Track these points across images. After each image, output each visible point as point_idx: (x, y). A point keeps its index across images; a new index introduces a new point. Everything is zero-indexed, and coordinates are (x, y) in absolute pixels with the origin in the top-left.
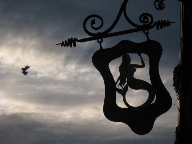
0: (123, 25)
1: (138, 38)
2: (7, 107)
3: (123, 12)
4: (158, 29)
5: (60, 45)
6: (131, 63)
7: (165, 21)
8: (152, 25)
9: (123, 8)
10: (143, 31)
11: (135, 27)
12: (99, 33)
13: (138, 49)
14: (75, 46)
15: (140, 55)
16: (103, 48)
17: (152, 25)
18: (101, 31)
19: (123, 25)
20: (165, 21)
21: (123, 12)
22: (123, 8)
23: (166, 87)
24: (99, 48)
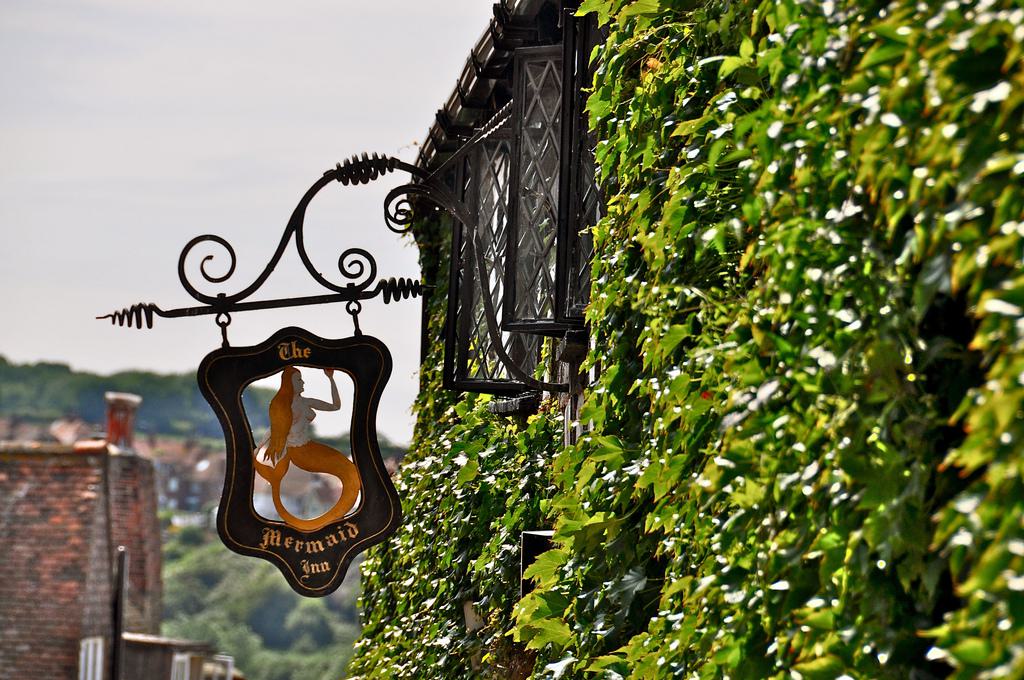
0: (292, 278)
1: (331, 323)
2: (142, 590)
3: (294, 233)
4: (387, 301)
5: (110, 318)
6: (302, 394)
7: (409, 280)
8: (372, 288)
9: (296, 223)
10: (215, 315)
11: (199, 300)
12: (222, 296)
13: (328, 354)
14: (150, 325)
15: (330, 376)
16: (232, 345)
17: (372, 288)
18: (230, 289)
19: (292, 278)
20: (402, 280)
21: (294, 233)
22: (296, 223)
23: (223, 434)
24: (218, 344)
